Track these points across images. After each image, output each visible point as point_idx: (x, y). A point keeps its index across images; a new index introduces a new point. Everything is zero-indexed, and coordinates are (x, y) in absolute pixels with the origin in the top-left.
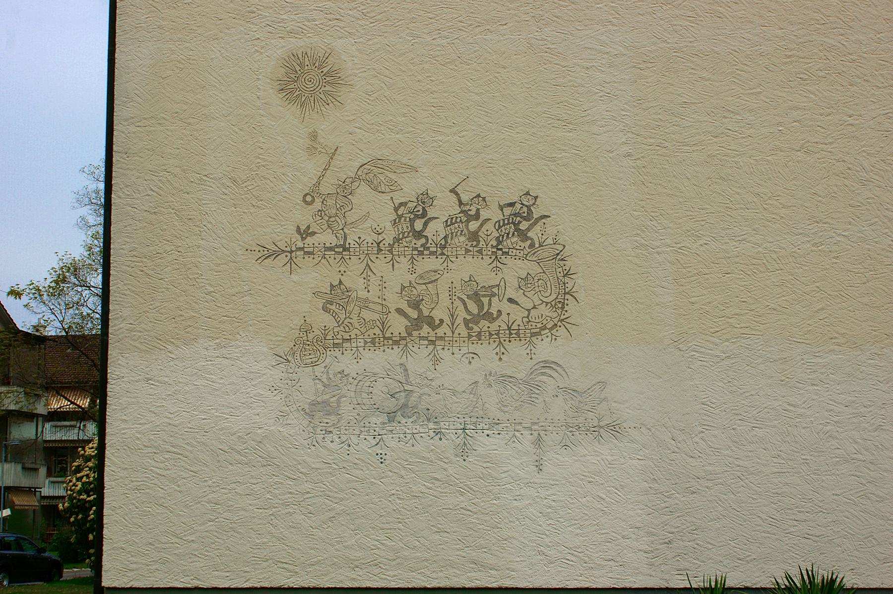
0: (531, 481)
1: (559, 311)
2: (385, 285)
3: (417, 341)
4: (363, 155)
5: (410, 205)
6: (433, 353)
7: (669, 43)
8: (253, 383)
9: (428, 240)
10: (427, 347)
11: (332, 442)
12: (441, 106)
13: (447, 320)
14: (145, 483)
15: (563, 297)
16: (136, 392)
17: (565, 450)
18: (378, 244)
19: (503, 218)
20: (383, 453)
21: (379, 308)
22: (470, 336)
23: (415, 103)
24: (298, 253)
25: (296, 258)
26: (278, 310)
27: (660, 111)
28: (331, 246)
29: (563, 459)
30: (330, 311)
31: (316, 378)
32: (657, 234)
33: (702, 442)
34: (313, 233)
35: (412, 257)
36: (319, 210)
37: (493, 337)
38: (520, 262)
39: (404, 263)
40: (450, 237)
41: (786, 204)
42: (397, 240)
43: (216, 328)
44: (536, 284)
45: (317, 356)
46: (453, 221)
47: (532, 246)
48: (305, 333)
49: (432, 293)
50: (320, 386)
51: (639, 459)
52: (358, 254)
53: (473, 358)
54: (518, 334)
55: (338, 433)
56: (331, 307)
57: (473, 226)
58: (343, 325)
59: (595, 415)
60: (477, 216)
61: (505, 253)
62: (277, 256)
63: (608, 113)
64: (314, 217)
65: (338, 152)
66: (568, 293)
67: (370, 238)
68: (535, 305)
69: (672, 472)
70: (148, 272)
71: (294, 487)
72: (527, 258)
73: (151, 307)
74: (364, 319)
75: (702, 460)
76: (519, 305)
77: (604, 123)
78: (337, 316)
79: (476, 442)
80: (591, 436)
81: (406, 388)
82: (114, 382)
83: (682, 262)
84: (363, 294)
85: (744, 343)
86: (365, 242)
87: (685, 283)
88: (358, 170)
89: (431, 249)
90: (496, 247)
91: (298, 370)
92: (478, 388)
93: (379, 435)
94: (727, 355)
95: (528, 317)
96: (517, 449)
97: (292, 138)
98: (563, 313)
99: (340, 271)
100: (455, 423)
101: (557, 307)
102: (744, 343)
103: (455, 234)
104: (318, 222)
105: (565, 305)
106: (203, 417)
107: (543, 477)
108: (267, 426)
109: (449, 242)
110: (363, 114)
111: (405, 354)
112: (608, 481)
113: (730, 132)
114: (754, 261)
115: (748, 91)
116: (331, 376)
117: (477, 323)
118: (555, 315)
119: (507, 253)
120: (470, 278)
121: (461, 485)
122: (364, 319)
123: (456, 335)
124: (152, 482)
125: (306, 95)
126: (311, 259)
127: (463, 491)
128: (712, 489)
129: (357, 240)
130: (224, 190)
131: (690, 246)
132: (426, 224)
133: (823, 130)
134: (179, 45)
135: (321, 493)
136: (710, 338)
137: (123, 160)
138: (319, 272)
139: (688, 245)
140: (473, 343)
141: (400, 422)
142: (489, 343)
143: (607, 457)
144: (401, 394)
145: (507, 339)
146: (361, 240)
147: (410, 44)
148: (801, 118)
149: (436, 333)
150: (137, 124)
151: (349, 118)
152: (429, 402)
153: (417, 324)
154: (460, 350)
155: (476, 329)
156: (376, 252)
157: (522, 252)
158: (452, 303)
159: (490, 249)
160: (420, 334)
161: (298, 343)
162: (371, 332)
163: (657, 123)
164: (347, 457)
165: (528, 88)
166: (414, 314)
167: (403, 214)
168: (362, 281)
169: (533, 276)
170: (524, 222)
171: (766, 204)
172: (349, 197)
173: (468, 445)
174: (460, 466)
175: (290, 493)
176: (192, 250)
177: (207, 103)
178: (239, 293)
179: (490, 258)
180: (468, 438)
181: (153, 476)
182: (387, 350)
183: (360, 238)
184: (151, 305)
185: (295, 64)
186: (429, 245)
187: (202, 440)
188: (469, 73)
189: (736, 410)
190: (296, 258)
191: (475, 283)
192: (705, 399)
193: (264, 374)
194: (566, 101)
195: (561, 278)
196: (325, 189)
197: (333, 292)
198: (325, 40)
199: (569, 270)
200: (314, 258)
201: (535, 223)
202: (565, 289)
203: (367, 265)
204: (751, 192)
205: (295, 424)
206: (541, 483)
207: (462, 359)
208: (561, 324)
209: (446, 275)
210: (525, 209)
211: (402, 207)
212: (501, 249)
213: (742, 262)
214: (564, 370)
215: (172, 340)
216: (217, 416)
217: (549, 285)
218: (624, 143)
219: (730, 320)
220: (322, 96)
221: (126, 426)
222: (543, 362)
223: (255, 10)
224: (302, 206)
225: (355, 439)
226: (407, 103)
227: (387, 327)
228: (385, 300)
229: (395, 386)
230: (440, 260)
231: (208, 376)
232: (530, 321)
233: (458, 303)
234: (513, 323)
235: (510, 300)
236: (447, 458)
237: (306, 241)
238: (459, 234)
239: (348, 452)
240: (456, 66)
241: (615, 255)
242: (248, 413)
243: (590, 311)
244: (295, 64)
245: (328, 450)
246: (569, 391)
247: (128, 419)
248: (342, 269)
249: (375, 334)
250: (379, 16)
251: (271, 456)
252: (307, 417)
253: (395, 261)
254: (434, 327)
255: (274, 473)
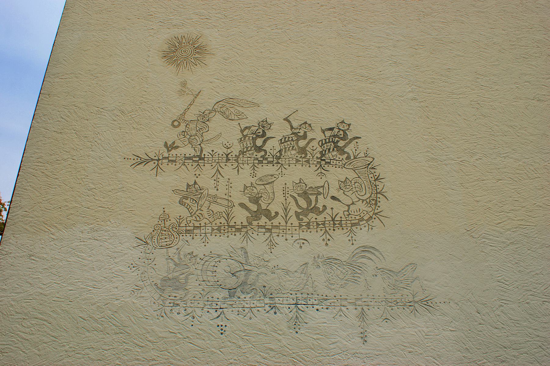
0: (358, 351)
1: (373, 207)
2: (231, 185)
3: (256, 229)
4: (219, 95)
5: (253, 128)
6: (270, 239)
7: (432, 35)
8: (116, 261)
9: (266, 153)
10: (264, 234)
11: (178, 313)
12: (277, 67)
13: (281, 213)
14: (9, 347)
15: (375, 196)
16: (18, 266)
17: (386, 323)
18: (227, 155)
19: (325, 138)
20: (224, 325)
21: (226, 203)
22: (300, 226)
23: (259, 65)
24: (164, 161)
25: (162, 164)
26: (143, 203)
27: (432, 73)
28: (190, 156)
29: (385, 331)
30: (185, 205)
31: (169, 258)
32: (443, 151)
33: (503, 314)
34: (177, 147)
35: (254, 165)
36: (183, 131)
37: (320, 226)
38: (339, 169)
39: (247, 169)
40: (284, 151)
41: (532, 133)
42: (242, 152)
43: (92, 216)
44: (354, 186)
45: (171, 239)
46: (287, 140)
47: (348, 158)
48: (163, 221)
49: (269, 191)
50: (172, 265)
51: (451, 331)
52: (211, 162)
53: (303, 243)
54: (340, 224)
55: (185, 306)
56: (186, 201)
57: (302, 143)
58: (195, 215)
59: (410, 291)
60: (305, 137)
61: (326, 163)
62: (147, 163)
63: (397, 74)
64: (179, 136)
65: (201, 94)
66: (379, 193)
67: (221, 151)
68: (353, 202)
69: (481, 341)
70: (47, 173)
71: (142, 354)
72: (345, 167)
73: (44, 199)
74: (213, 211)
75: (505, 331)
76: (340, 201)
77: (394, 79)
78: (190, 208)
79: (308, 316)
80: (408, 310)
81: (246, 268)
82: (3, 257)
83: (464, 171)
84: (212, 192)
85: (522, 232)
86: (217, 154)
87: (469, 186)
88: (215, 105)
89: (269, 159)
90: (320, 158)
91: (155, 251)
92: (308, 268)
93: (221, 308)
94: (511, 241)
95: (348, 211)
96: (344, 322)
97: (168, 85)
98: (376, 208)
99: (195, 175)
100: (288, 299)
101: (371, 203)
102: (522, 232)
103: (287, 149)
104: (181, 140)
105: (378, 202)
106: (70, 288)
107: (368, 348)
108: (124, 298)
109: (283, 154)
110: (221, 71)
111: (245, 239)
112: (426, 351)
113: (483, 87)
114: (518, 171)
115: (490, 64)
116: (182, 257)
117: (306, 216)
118: (370, 209)
119: (329, 163)
120: (300, 180)
121: (294, 355)
122: (213, 211)
123: (289, 224)
124: (16, 345)
125: (181, 60)
126: (173, 165)
127: (296, 361)
128: (518, 358)
129: (211, 152)
130: (114, 118)
131: (469, 160)
132: (265, 142)
133: (546, 88)
134: (99, 32)
135: (165, 361)
136: (495, 228)
137: (46, 99)
138: (179, 175)
139: (467, 159)
140: (303, 231)
141: (239, 298)
142: (317, 231)
143: (423, 329)
144: (242, 273)
145: (332, 228)
146: (214, 152)
147: (256, 32)
148: (530, 80)
149: (272, 223)
150: (61, 77)
151: (210, 73)
152: (265, 280)
153: (256, 215)
154: (292, 237)
155: (305, 220)
156: (225, 161)
157: (341, 162)
158: (286, 199)
159: (316, 160)
160: (258, 223)
161: (156, 229)
162: (218, 221)
163: (431, 80)
164: (191, 327)
165: (339, 57)
166: (254, 208)
167: (247, 134)
168: (213, 182)
169: (351, 180)
170: (341, 141)
171: (518, 133)
172: (207, 123)
173: (300, 319)
174: (292, 338)
175: (138, 360)
176: (84, 158)
177: (112, 65)
178: (114, 189)
179: (316, 166)
180: (300, 312)
181: (18, 340)
182: (231, 236)
183: (213, 151)
184: (45, 197)
185: (176, 42)
186: (267, 156)
187: (67, 308)
188: (297, 48)
189: (526, 286)
190: (162, 164)
191: (304, 185)
192: (500, 278)
193: (126, 254)
194: (366, 66)
195: (373, 182)
196: (188, 117)
197: (188, 190)
198: (198, 30)
199: (379, 176)
200: (175, 165)
201: (350, 142)
202: (376, 190)
203: (218, 170)
204: (506, 125)
205: (148, 297)
206: (366, 354)
207: (294, 244)
208: (375, 217)
209: (280, 178)
210: (341, 132)
211: (246, 130)
212: (324, 160)
213: (509, 172)
214: (381, 254)
215: (55, 225)
216: (82, 288)
217: (363, 187)
218: (410, 92)
219: (508, 214)
220: (193, 60)
221: (4, 295)
222: (362, 247)
223: (153, 14)
224: (170, 128)
225: (199, 312)
226: (253, 65)
227: (231, 218)
228: (230, 196)
229: (236, 266)
230: (276, 167)
231: (79, 254)
232: (350, 214)
233: (290, 200)
234: (336, 216)
235: (333, 198)
236: (281, 330)
237: (171, 153)
238: (291, 149)
239: (192, 323)
240: (288, 44)
241: (413, 165)
242: (109, 286)
243: (398, 207)
244: (176, 42)
245: (175, 320)
246: (386, 271)
247: (7, 288)
248: (197, 173)
249: (221, 223)
250: (235, 17)
251: (124, 325)
252: (158, 291)
253: (239, 168)
254: (270, 218)
255: (125, 341)
